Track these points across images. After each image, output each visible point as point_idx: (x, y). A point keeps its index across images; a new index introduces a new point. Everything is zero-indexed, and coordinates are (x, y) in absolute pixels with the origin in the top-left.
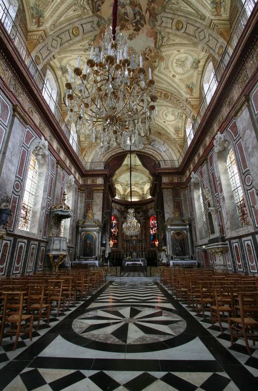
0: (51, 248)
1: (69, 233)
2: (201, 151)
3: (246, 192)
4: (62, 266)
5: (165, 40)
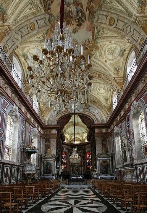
0: (26, 169)
2: (122, 113)
4: (33, 179)
5: (100, 33)
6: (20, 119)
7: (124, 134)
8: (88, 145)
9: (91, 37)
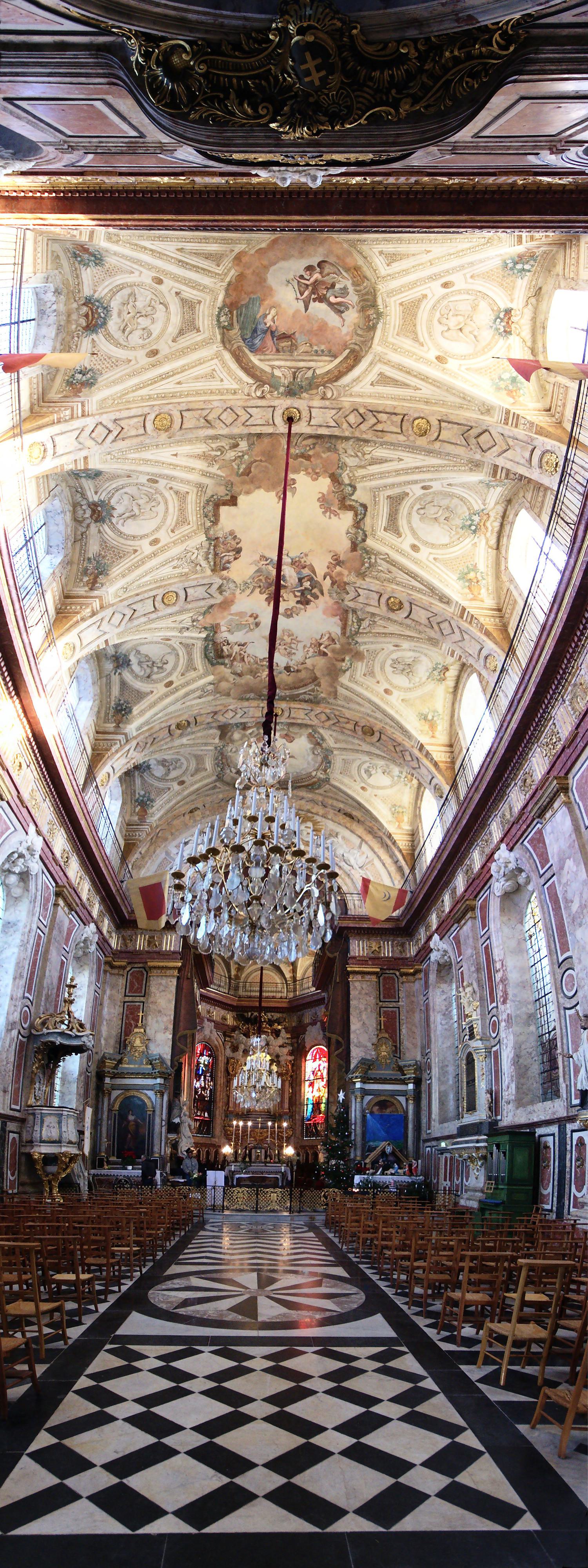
0: (36, 1135)
1: (78, 1094)
2: (460, 882)
3: (562, 1012)
4: (68, 1185)
5: (365, 624)
6: (40, 887)
7: (470, 976)
8: (313, 1010)
9: (336, 630)
